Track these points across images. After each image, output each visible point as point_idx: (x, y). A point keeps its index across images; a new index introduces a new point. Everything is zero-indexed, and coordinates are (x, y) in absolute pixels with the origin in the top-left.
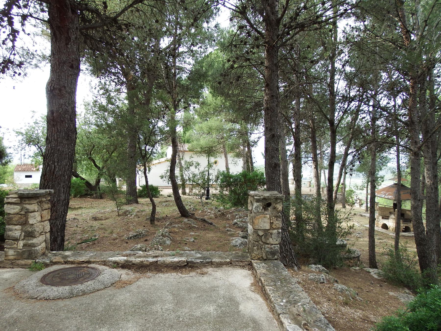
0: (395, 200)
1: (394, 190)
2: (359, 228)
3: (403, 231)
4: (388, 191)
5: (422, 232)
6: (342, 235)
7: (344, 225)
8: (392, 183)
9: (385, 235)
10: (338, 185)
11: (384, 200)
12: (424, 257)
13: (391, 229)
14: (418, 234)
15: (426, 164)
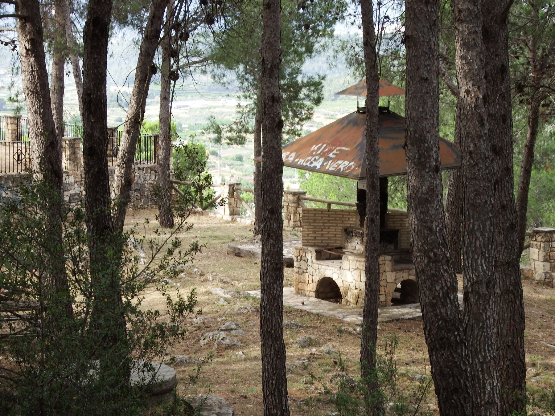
0: (361, 178)
1: (359, 135)
2: (227, 308)
3: (396, 302)
4: (335, 143)
5: (447, 295)
6: (147, 345)
7: (151, 299)
8: (352, 105)
9: (329, 326)
10: (136, 121)
11: (317, 182)
12: (456, 390)
13: (350, 298)
14: (433, 306)
15: (461, 21)
